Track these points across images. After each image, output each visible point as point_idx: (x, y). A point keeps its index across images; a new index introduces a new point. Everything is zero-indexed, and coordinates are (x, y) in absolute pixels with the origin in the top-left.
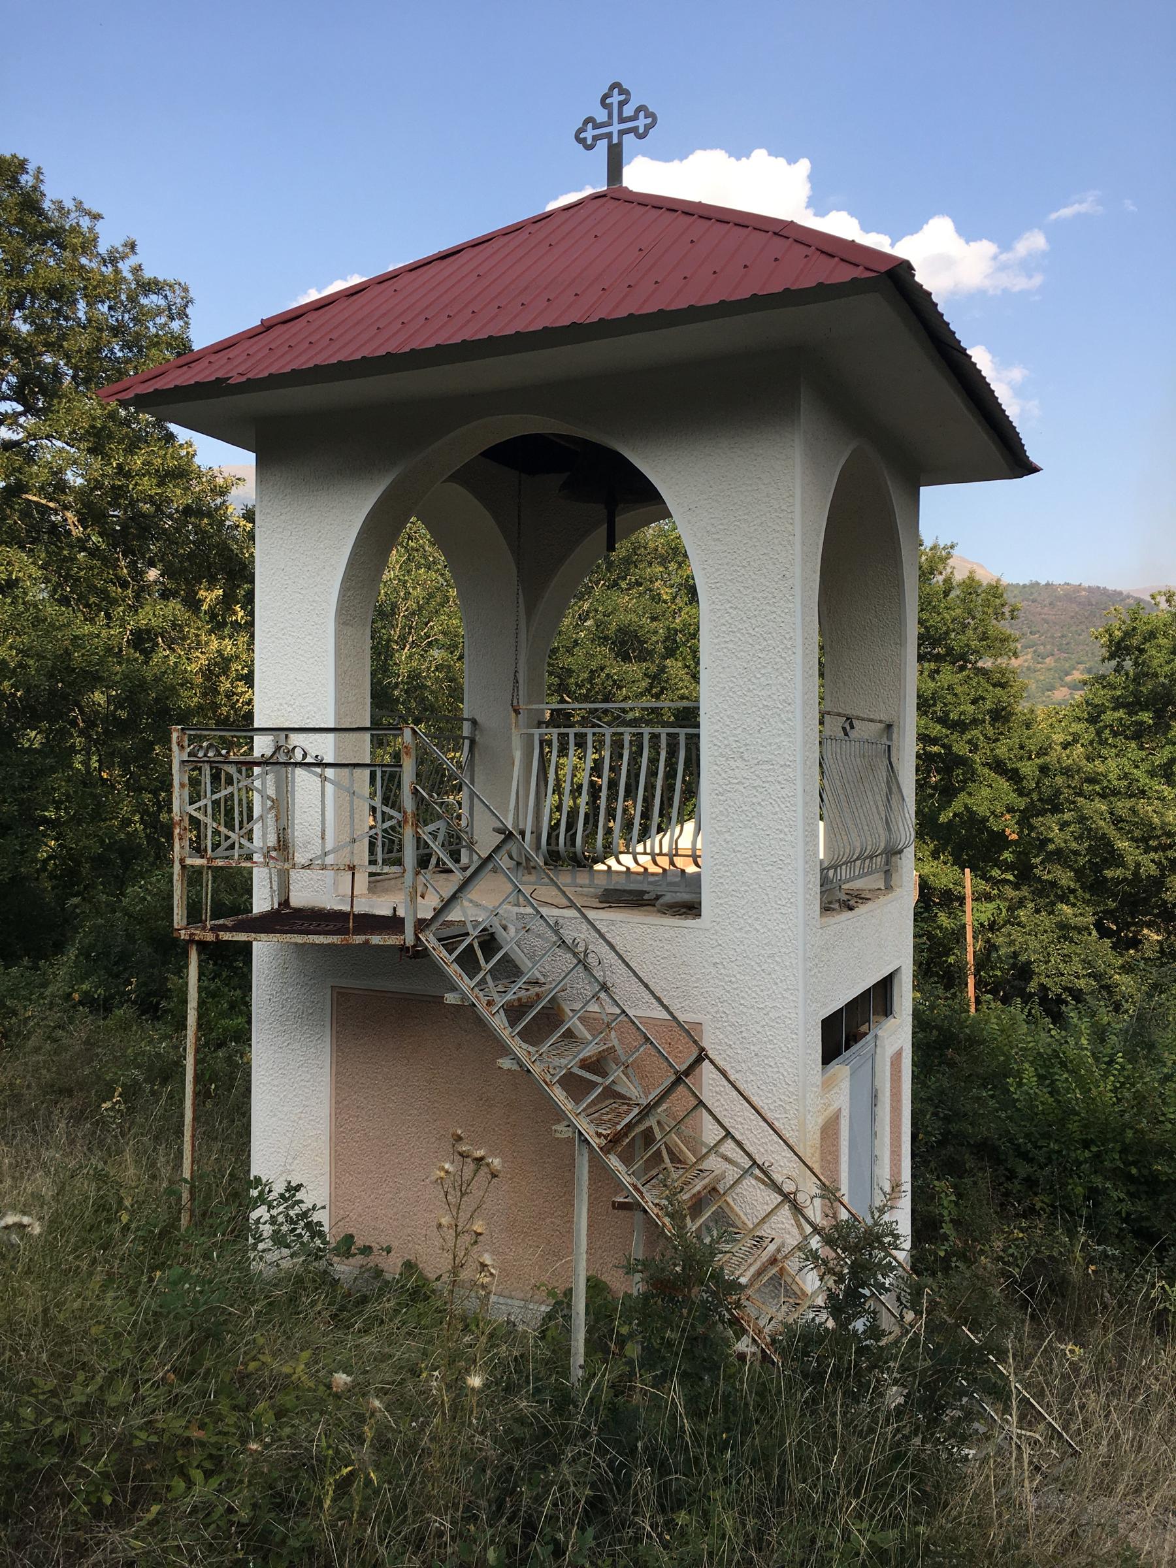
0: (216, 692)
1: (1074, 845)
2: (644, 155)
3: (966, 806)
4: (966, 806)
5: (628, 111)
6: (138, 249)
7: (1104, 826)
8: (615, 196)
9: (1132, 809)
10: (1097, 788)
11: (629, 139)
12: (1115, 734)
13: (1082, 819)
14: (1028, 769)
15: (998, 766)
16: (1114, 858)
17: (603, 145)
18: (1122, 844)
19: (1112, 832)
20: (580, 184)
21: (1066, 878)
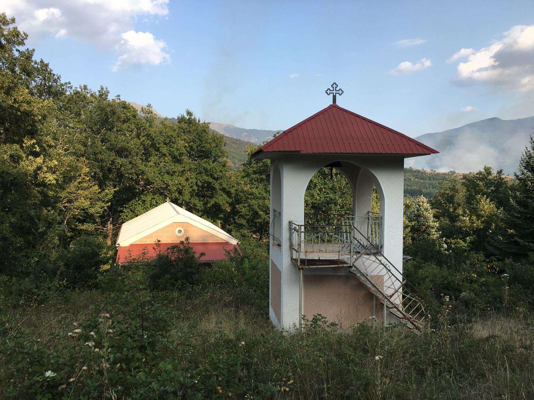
0: (293, 372)
1: (248, 213)
2: (141, 32)
3: (215, 202)
4: (215, 202)
5: (332, 89)
6: (16, 20)
7: (256, 207)
8: (334, 107)
9: (111, 145)
10: (252, 197)
11: (337, 95)
12: (255, 181)
13: (249, 206)
14: (233, 191)
15: (224, 190)
16: (259, 216)
17: (332, 95)
18: (261, 213)
19: (258, 210)
20: (328, 102)
21: (243, 222)
